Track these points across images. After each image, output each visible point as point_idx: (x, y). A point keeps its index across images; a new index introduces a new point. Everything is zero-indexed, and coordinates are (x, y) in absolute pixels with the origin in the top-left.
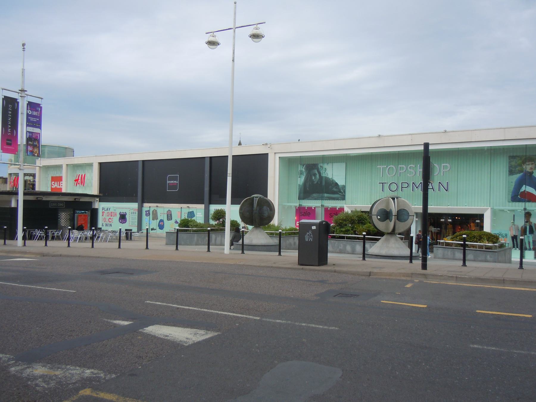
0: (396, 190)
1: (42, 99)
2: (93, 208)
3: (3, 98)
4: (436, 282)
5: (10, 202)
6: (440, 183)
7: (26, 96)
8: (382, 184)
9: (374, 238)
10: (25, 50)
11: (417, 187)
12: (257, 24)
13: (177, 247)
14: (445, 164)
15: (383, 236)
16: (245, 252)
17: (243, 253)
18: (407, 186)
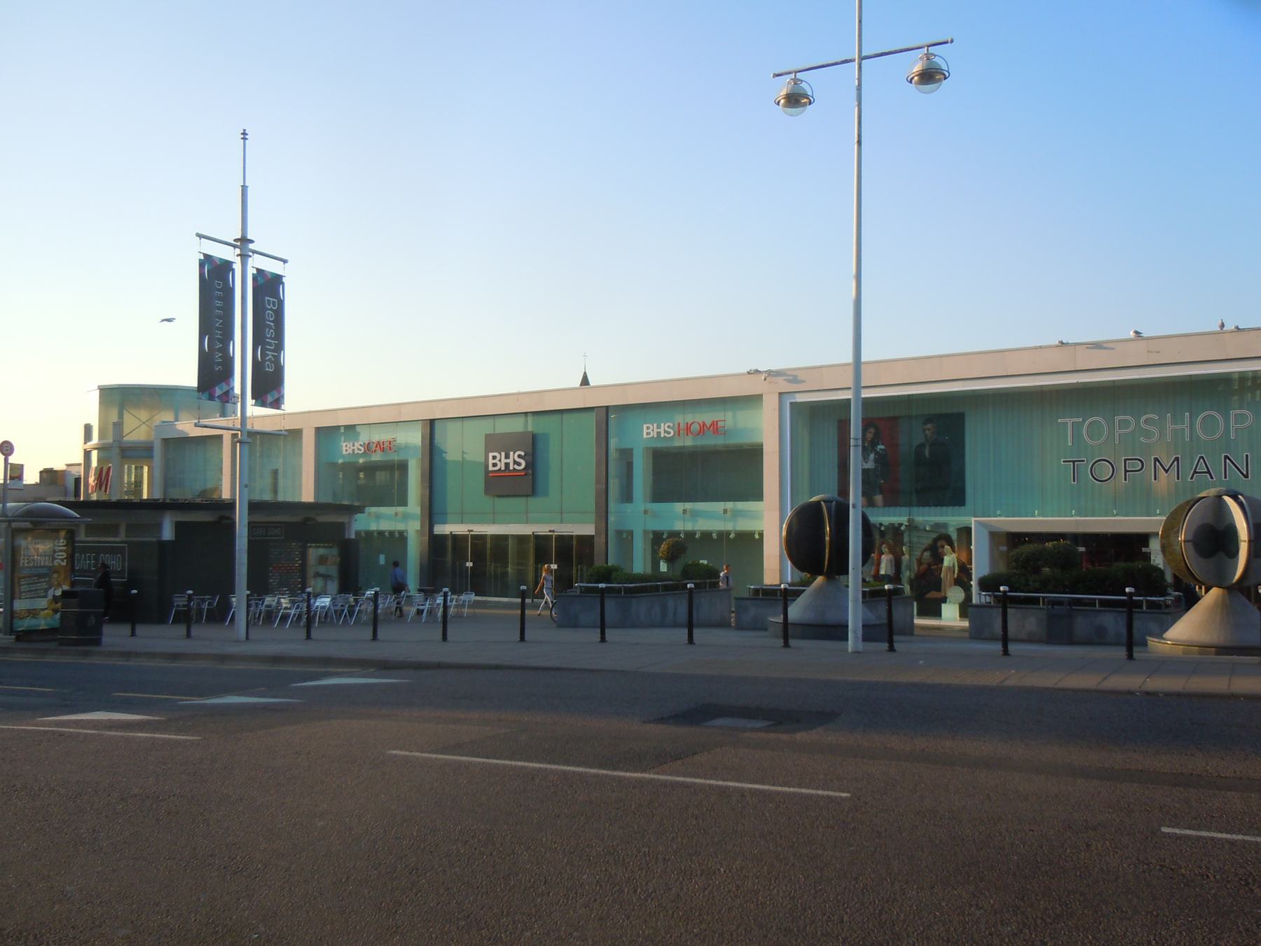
0: (1107, 480)
1: (285, 261)
2: (347, 537)
3: (200, 260)
4: (69, 637)
5: (159, 526)
6: (1156, 460)
7: (251, 254)
8: (1072, 463)
9: (1114, 600)
10: (242, 136)
11: (1197, 470)
12: (928, 46)
13: (603, 633)
14: (1122, 417)
15: (808, 586)
16: (792, 642)
17: (786, 645)
18: (1139, 468)
